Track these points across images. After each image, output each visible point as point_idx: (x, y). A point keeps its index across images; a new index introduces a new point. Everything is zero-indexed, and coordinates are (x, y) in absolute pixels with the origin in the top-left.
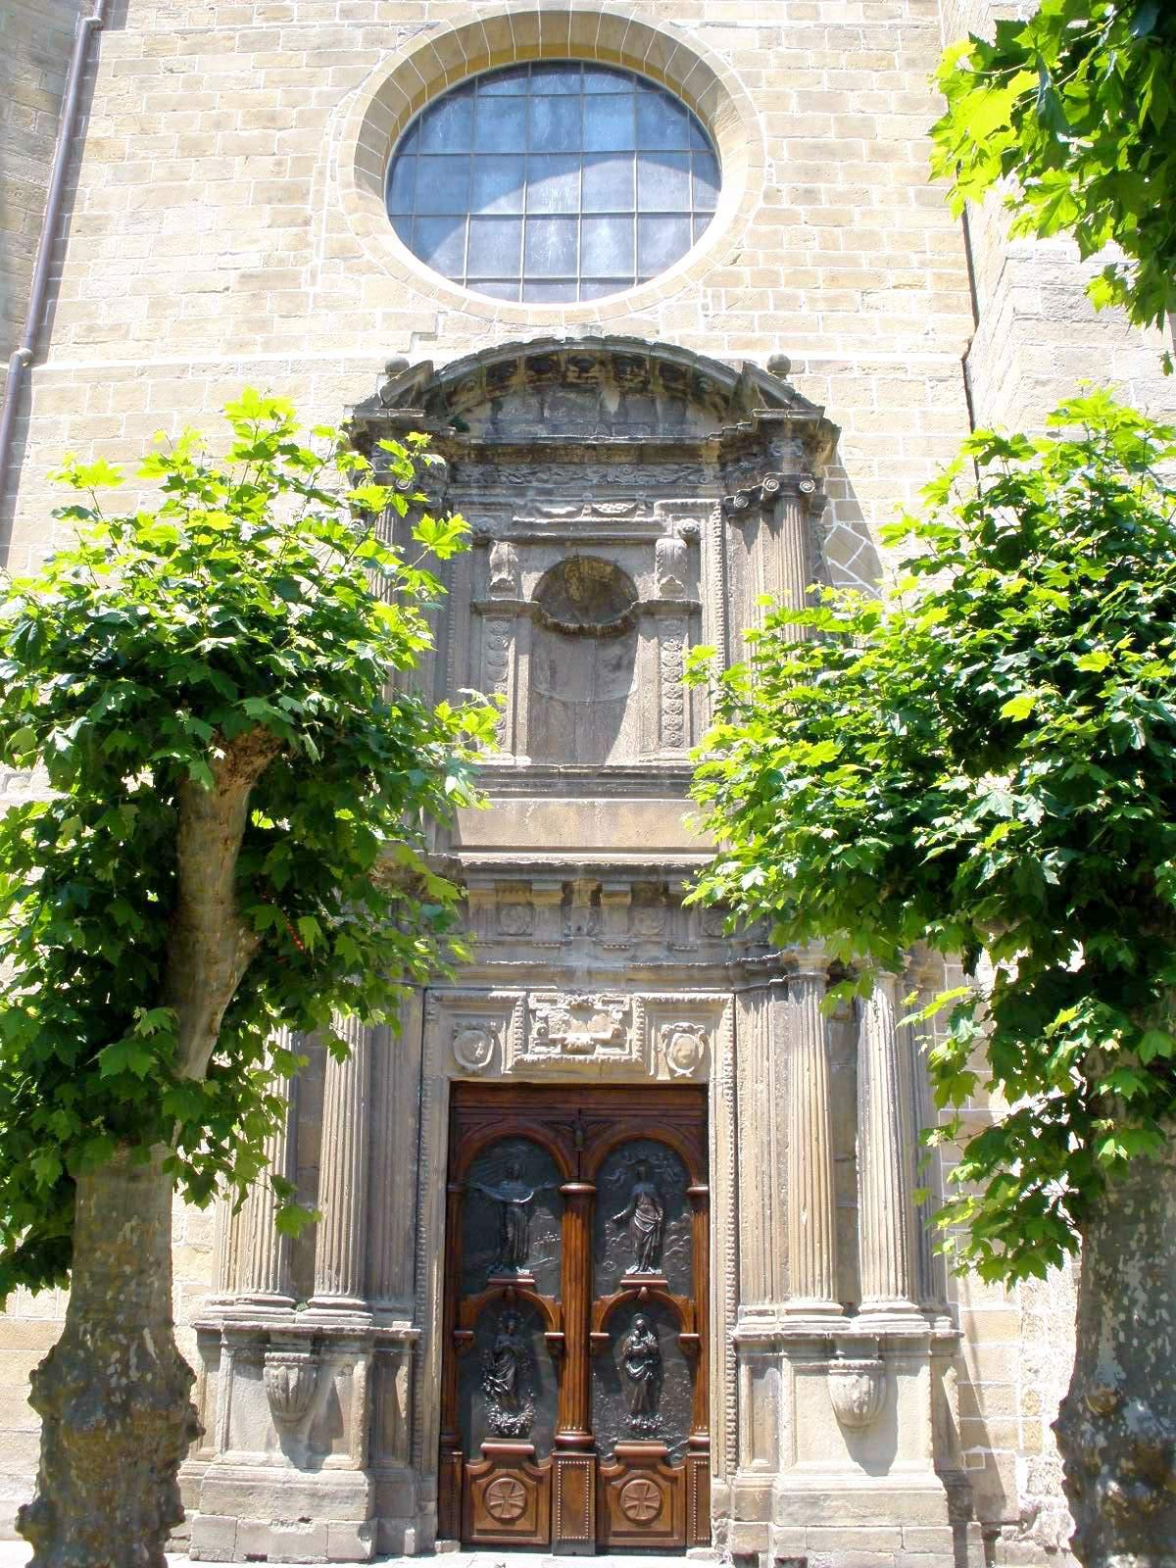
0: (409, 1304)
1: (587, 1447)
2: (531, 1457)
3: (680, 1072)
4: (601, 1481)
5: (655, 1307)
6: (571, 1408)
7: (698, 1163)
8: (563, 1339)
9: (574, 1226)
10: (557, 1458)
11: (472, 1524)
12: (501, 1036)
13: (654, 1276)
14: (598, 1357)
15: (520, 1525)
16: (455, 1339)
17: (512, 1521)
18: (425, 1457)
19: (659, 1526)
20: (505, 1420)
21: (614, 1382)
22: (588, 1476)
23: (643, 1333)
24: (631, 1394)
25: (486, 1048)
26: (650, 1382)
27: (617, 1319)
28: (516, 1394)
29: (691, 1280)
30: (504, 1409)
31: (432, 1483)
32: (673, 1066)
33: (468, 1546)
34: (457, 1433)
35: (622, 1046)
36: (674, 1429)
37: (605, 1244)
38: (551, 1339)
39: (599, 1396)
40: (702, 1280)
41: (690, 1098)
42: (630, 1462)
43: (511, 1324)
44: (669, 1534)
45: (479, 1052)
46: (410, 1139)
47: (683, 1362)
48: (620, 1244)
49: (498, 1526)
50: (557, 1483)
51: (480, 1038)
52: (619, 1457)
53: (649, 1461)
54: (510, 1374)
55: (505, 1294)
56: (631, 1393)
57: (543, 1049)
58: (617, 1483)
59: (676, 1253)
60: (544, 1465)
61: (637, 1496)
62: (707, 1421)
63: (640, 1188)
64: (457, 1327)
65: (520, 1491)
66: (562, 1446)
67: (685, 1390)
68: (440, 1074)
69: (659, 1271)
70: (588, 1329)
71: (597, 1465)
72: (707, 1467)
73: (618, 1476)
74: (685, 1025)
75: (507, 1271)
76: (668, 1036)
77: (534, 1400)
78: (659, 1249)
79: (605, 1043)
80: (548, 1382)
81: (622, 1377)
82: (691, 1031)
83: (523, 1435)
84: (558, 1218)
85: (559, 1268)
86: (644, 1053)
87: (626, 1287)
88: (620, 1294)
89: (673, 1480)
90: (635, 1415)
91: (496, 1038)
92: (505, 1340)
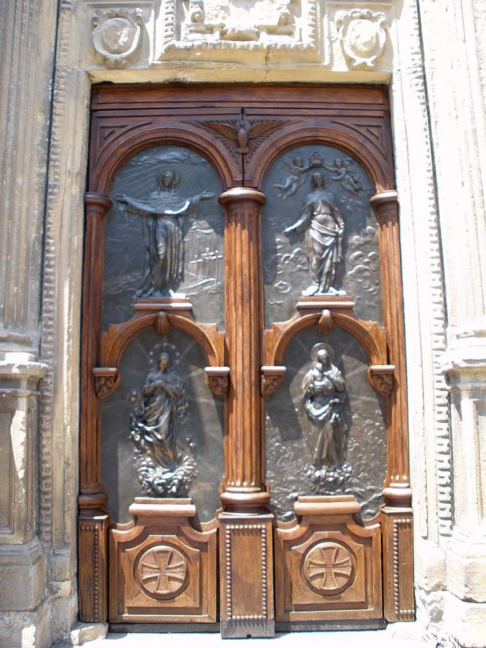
0: (33, 334)
1: (263, 507)
2: (193, 521)
3: (359, 60)
4: (280, 546)
5: (338, 334)
6: (239, 456)
7: (385, 169)
8: (228, 376)
9: (238, 237)
10: (225, 521)
11: (121, 601)
12: (149, 26)
13: (337, 298)
14: (272, 395)
15: (181, 601)
16: (95, 379)
17: (171, 597)
18: (57, 525)
19: (349, 597)
20: (158, 475)
21: (292, 426)
22: (265, 544)
23: (326, 367)
24: (314, 440)
25: (131, 36)
26: (336, 425)
27: (295, 350)
28: (172, 444)
29: (379, 302)
30: (157, 462)
31: (66, 560)
32: (351, 54)
33: (116, 628)
34: (100, 493)
35: (290, 34)
36: (365, 480)
37: (276, 262)
38: (214, 377)
39: (274, 443)
40: (395, 301)
41: (373, 96)
42: (313, 523)
43: (164, 358)
44: (363, 605)
45: (123, 39)
46: (39, 138)
47: (375, 400)
48: (295, 261)
49: (154, 603)
50: (225, 552)
51: (124, 25)
52: (300, 518)
53: (340, 519)
54: (164, 419)
55: (155, 324)
56: (314, 439)
57: (199, 36)
58: (300, 548)
59: (360, 271)
60: (208, 529)
61: (323, 562)
62: (406, 470)
63: (316, 197)
64: (98, 365)
65: (179, 561)
66: (230, 506)
67: (378, 434)
68: (79, 69)
69: (342, 293)
70: (259, 364)
71: (274, 527)
72: (410, 525)
73: (300, 540)
74: (364, 12)
75: (158, 295)
76: (343, 24)
77: (193, 451)
78: (340, 266)
79: (271, 31)
80: (212, 430)
81: (302, 420)
82: (370, 17)
83: (182, 492)
84: (221, 233)
85: (220, 291)
86: (316, 35)
87: (303, 310)
88: (296, 319)
89: (367, 541)
90: (318, 465)
91: (142, 27)
92: (156, 378)
